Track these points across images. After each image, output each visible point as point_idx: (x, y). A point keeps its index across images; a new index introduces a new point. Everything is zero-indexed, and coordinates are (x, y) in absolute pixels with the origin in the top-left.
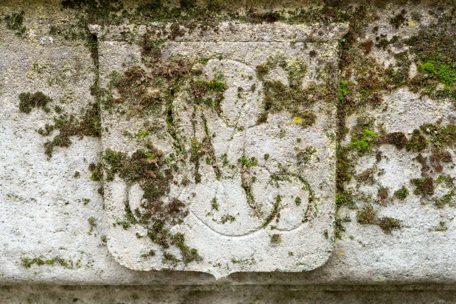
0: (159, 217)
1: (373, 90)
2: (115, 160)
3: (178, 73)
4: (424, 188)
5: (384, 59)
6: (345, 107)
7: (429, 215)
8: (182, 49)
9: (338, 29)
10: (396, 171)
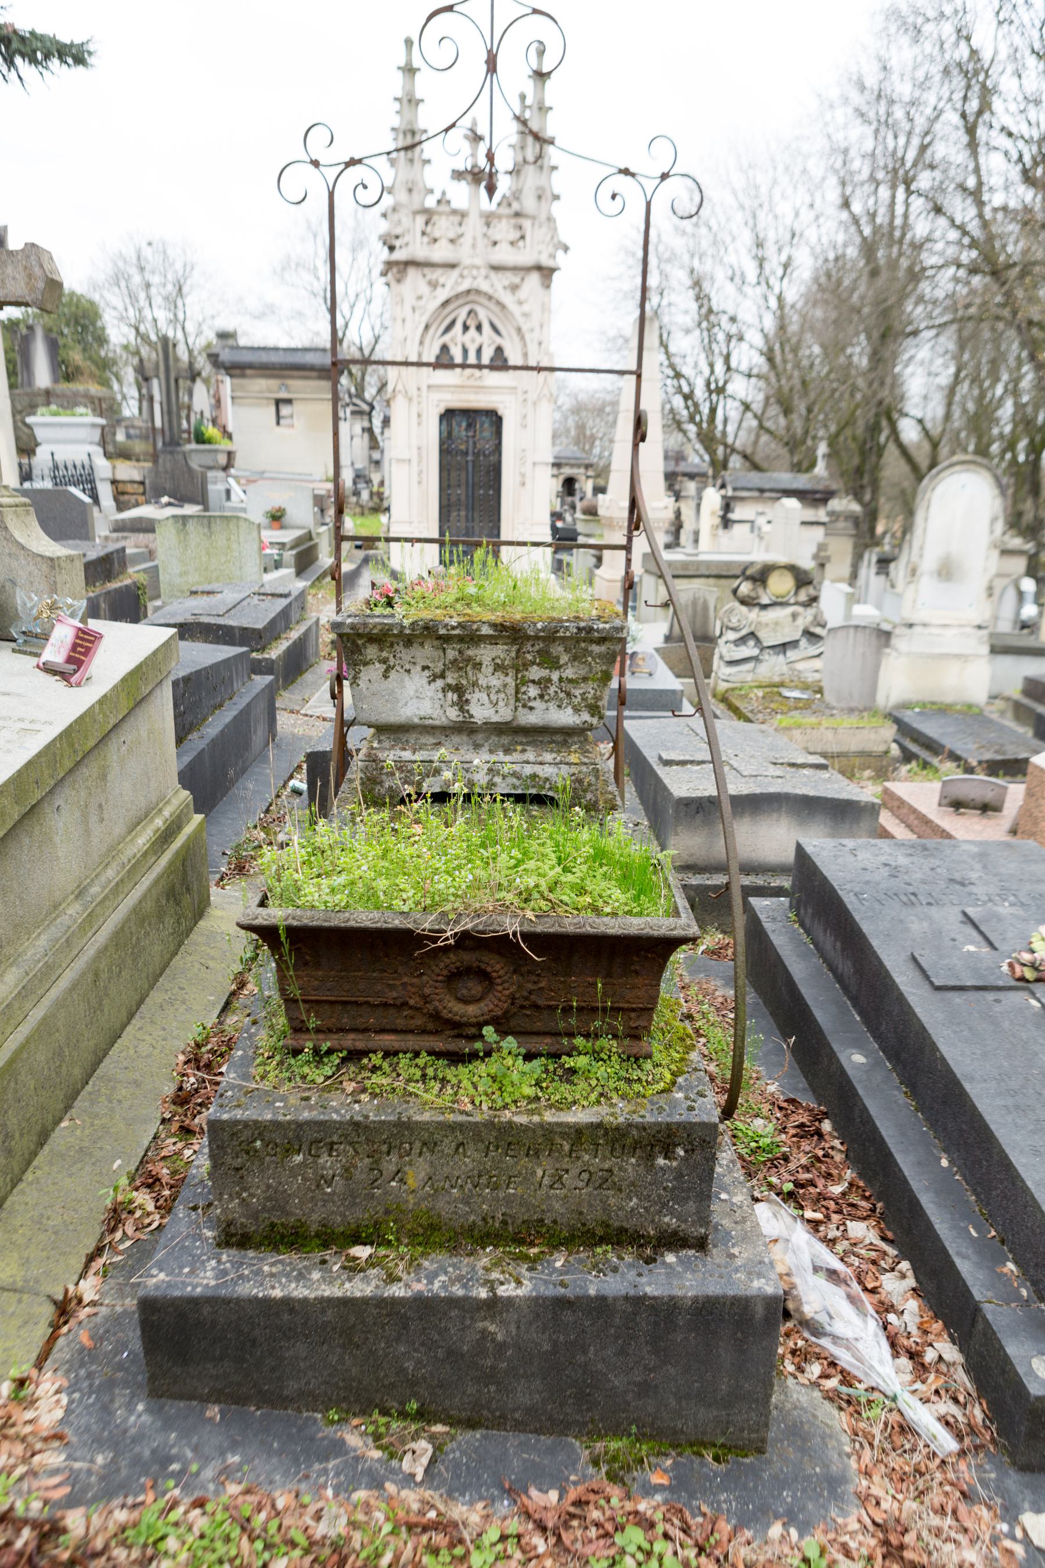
0: (462, 704)
1: (526, 666)
2: (449, 686)
3: (469, 659)
4: (541, 696)
5: (529, 657)
6: (518, 671)
7: (543, 705)
8: (470, 653)
9: (515, 648)
10: (533, 691)
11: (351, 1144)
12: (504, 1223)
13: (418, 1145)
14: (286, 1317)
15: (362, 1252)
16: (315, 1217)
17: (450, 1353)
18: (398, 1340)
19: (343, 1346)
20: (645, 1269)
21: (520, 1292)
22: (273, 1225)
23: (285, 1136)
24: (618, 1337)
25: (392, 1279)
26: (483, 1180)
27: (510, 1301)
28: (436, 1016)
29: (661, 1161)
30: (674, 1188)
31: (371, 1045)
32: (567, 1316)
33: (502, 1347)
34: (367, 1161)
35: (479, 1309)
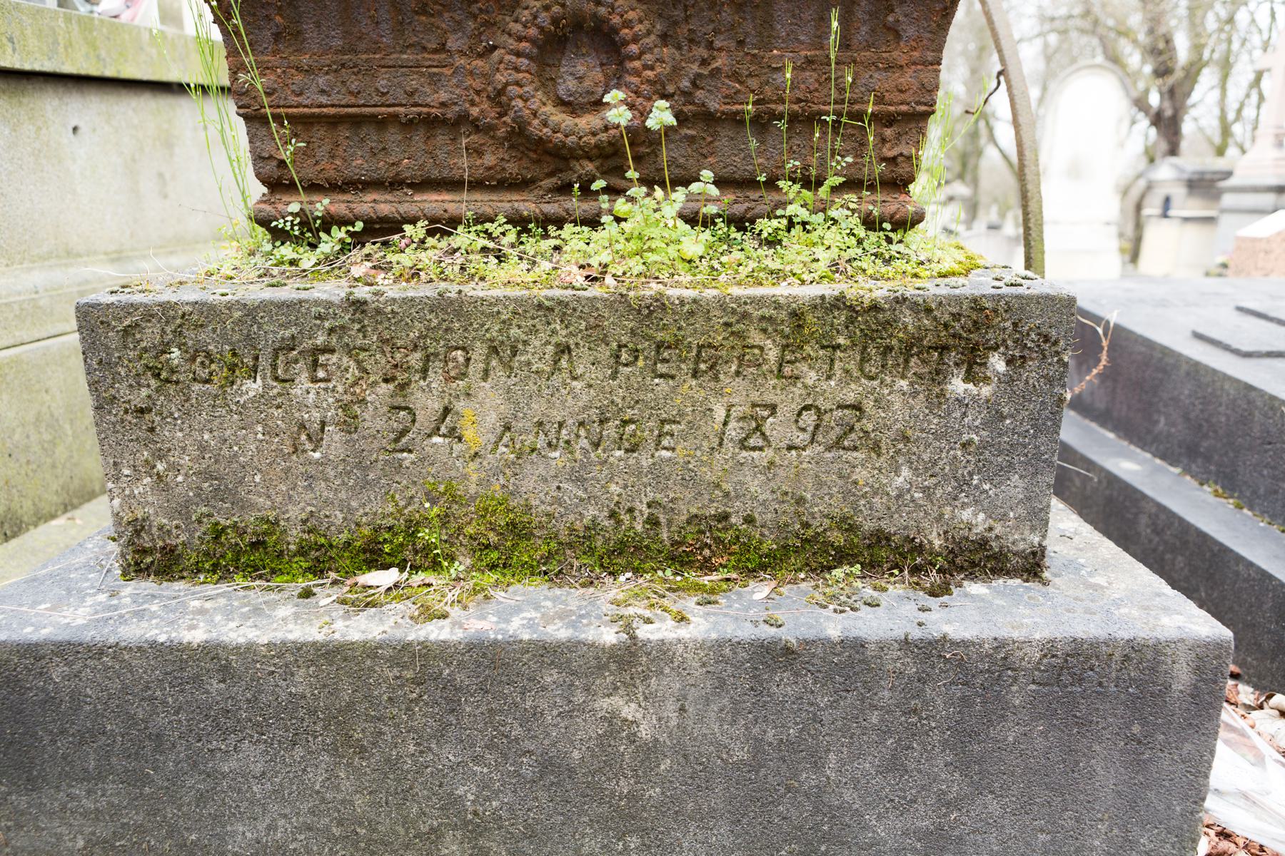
11: (349, 351)
12: (653, 522)
13: (479, 351)
14: (215, 686)
15: (383, 578)
16: (295, 512)
17: (547, 765)
18: (440, 736)
19: (334, 751)
20: (933, 602)
21: (684, 633)
22: (218, 533)
23: (225, 338)
24: (885, 732)
25: (428, 614)
26: (611, 430)
27: (663, 651)
28: (520, 139)
29: (958, 385)
30: (984, 446)
31: (406, 208)
32: (783, 686)
33: (650, 752)
34: (385, 389)
35: (601, 668)
